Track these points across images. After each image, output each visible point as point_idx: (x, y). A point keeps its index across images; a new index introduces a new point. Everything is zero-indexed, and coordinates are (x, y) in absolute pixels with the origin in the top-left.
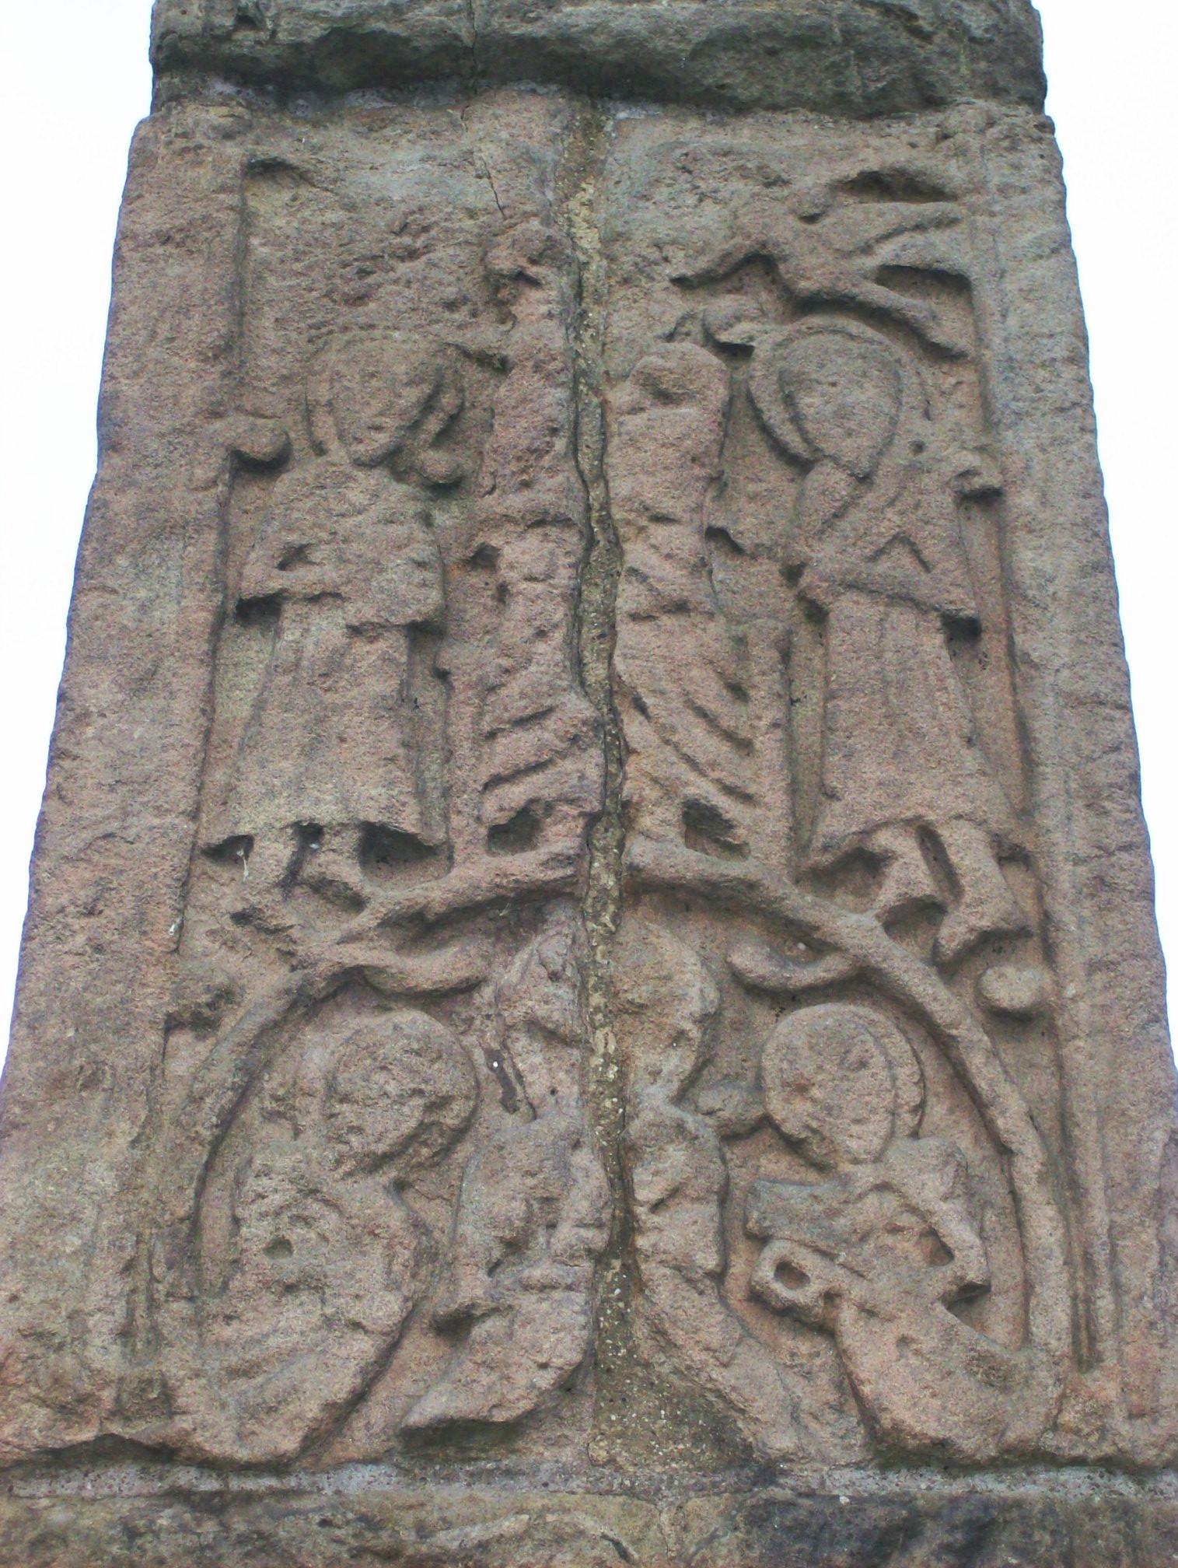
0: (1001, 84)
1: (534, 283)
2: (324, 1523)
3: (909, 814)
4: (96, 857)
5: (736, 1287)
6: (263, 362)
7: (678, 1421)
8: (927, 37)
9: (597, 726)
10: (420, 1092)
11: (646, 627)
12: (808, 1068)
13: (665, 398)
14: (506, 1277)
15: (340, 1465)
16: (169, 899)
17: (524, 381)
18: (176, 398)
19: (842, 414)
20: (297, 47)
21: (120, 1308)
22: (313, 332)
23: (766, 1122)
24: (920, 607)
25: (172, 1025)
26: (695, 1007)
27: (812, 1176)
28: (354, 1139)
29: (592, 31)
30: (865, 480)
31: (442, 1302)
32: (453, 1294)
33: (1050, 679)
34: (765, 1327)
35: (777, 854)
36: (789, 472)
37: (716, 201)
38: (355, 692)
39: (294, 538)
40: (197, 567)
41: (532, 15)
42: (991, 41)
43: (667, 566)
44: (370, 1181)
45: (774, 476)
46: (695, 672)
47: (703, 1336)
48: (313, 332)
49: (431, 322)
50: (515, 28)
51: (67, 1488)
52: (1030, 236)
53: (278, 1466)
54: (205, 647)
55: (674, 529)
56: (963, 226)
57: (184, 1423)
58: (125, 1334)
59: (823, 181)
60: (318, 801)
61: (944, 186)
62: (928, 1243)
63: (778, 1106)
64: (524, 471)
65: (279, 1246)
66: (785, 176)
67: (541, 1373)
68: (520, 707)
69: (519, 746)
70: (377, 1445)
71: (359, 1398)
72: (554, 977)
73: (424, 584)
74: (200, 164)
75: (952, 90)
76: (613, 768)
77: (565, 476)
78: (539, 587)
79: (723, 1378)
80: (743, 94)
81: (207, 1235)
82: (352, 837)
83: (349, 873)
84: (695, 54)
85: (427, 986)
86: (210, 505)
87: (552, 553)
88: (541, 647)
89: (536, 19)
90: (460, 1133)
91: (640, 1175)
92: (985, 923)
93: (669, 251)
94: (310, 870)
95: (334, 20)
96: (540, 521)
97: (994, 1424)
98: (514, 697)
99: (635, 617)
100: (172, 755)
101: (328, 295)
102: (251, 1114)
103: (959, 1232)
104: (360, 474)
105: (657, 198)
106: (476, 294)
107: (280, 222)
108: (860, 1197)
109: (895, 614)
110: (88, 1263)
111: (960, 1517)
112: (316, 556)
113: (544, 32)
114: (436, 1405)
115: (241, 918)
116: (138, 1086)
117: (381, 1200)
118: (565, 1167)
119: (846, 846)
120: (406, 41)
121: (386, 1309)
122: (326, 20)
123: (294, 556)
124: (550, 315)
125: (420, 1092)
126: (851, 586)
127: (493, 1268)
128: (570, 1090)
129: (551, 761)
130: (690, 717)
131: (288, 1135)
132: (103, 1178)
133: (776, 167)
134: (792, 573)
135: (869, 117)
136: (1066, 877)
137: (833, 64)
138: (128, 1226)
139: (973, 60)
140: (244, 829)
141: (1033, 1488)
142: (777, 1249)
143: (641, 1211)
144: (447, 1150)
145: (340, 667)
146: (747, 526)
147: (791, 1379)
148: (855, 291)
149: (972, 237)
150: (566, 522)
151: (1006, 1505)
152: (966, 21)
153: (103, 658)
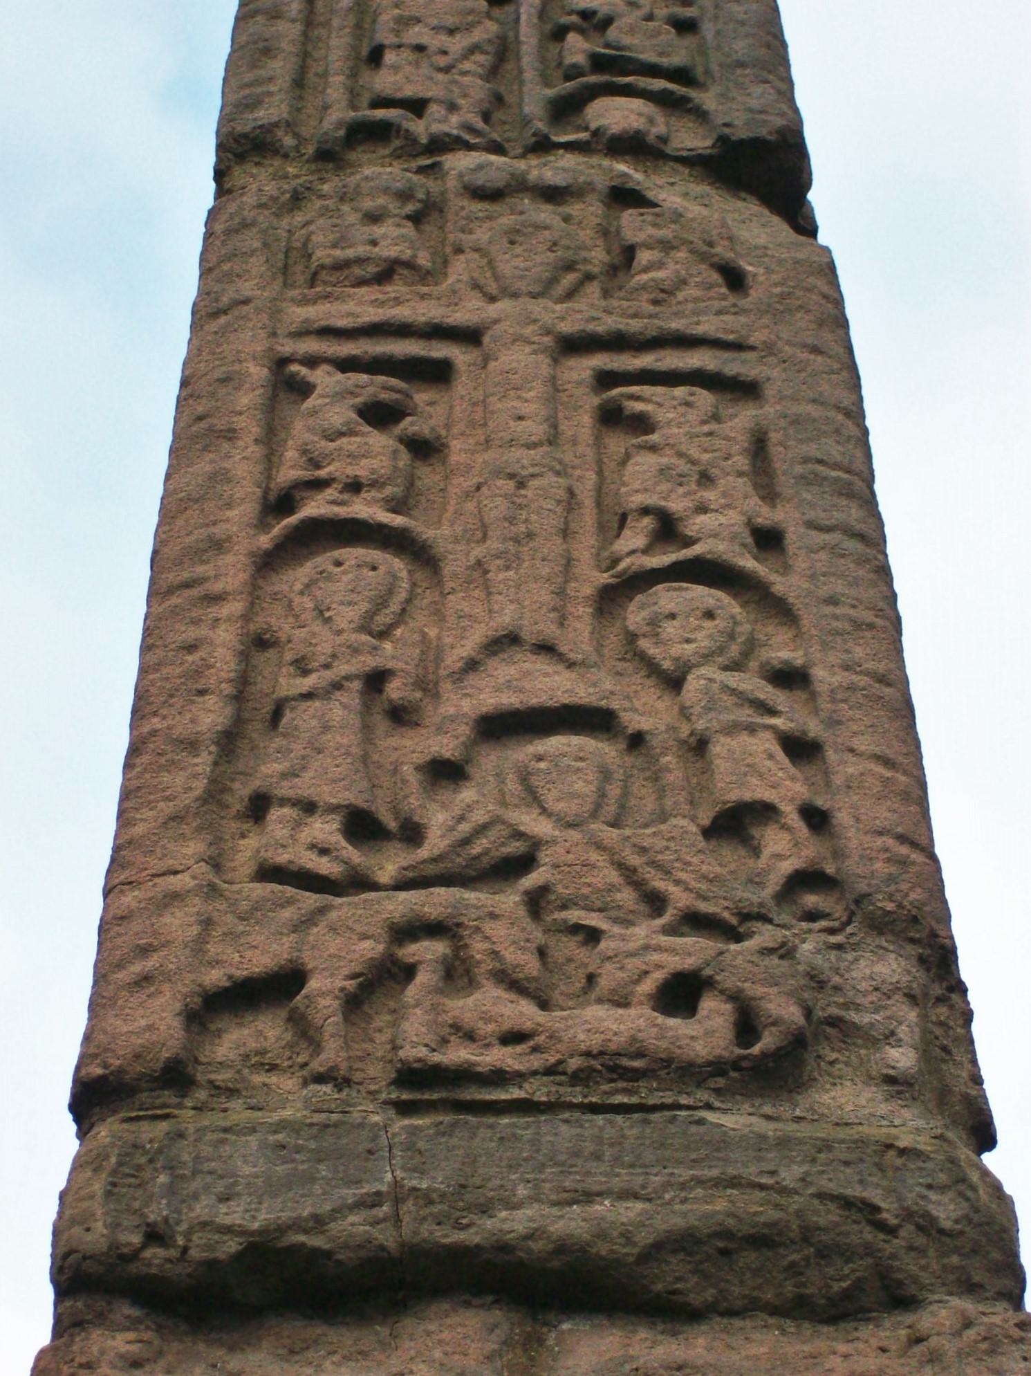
8: (892, 1231)
20: (212, 1264)
42: (962, 1233)
50: (446, 1236)
75: (922, 1287)
80: (695, 1299)
95: (252, 1233)
113: (477, 1239)
120: (328, 1254)
137: (792, 1265)
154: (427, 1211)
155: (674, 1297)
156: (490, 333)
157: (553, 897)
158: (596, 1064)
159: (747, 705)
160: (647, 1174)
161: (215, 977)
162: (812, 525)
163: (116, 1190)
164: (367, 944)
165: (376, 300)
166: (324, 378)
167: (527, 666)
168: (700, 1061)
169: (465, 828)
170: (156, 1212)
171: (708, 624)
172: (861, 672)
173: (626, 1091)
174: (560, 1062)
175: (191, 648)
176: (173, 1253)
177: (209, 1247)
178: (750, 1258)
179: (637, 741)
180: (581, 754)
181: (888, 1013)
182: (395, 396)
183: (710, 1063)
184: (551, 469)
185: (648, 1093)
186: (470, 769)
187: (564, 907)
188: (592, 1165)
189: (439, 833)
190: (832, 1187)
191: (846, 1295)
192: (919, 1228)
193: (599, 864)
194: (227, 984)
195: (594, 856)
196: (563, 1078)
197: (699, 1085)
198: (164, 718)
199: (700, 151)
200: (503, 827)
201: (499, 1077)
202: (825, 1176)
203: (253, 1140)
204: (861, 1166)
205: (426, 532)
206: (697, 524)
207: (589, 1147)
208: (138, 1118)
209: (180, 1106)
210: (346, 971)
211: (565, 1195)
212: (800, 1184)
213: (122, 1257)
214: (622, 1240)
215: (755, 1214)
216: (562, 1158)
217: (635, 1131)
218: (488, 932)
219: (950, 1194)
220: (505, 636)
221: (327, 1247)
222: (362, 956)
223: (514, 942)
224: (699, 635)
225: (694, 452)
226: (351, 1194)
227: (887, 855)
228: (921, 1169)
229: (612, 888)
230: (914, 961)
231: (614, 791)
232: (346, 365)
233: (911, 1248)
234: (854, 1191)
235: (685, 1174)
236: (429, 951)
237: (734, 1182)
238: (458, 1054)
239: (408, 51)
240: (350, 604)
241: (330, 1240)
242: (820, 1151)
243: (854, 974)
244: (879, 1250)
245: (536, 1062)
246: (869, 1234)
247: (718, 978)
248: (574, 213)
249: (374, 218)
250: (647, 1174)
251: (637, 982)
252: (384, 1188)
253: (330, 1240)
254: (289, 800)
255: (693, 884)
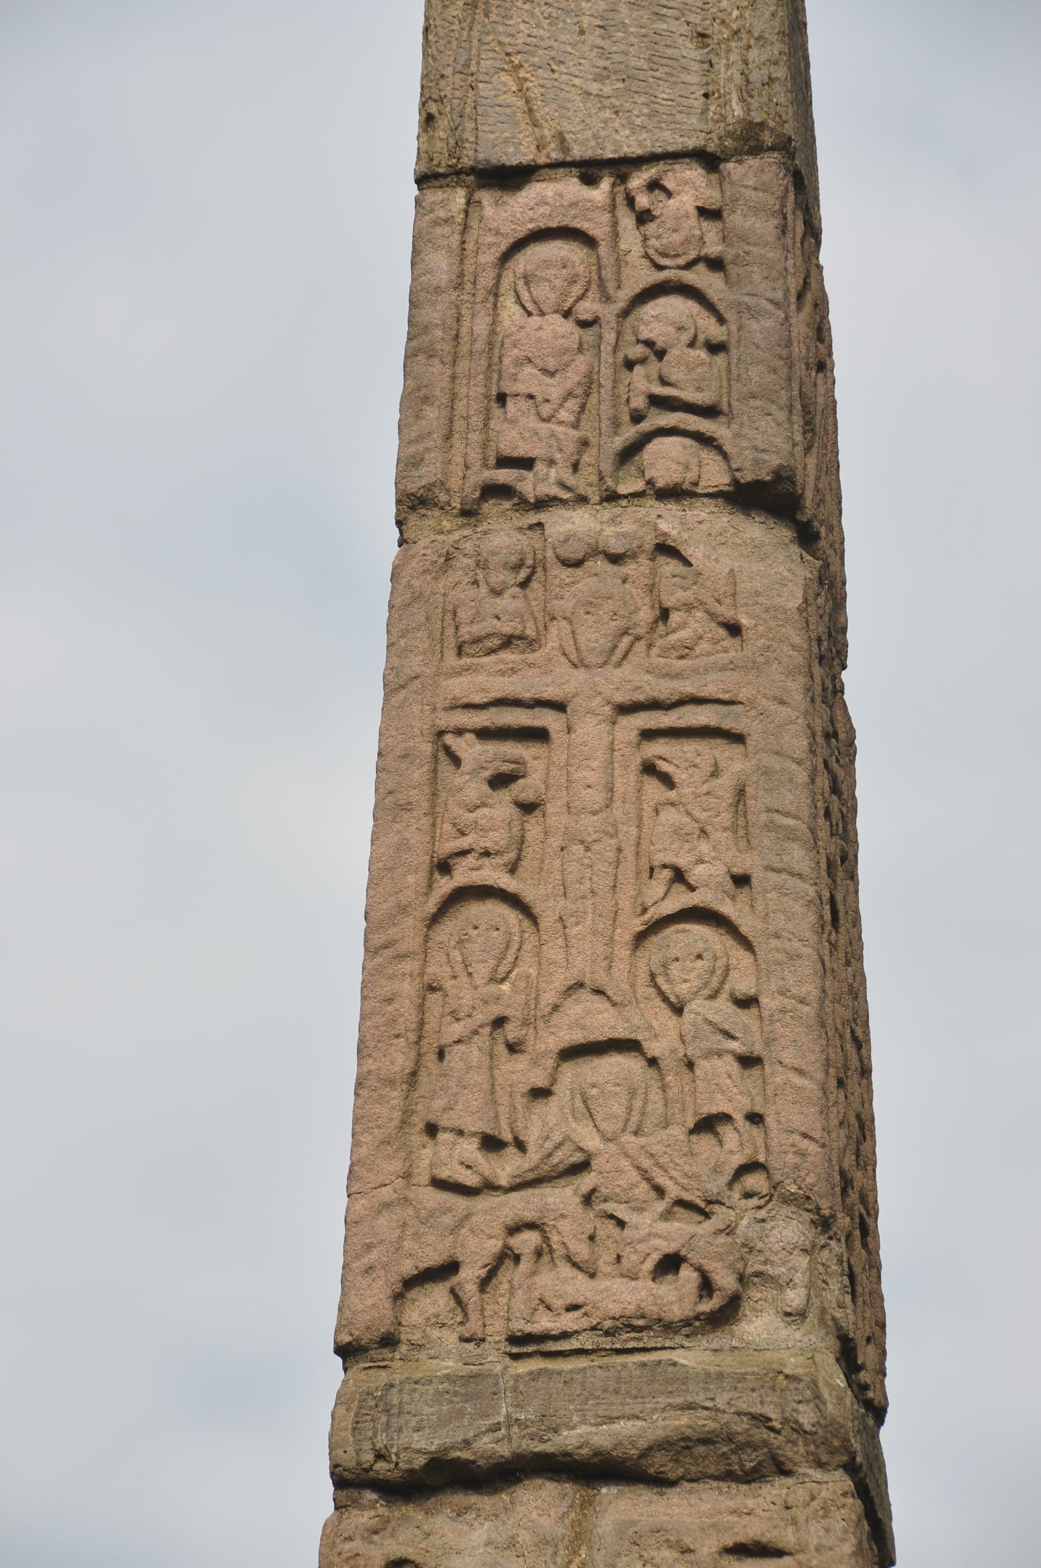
8: (778, 1432)
20: (412, 1471)
29: (579, 1447)
41: (545, 1438)
42: (816, 1433)
44: (534, 1245)
50: (536, 1447)
59: (714, 1550)
61: (784, 1547)
66: (692, 1547)
67: (670, 1247)
75: (795, 1464)
80: (672, 1476)
89: (549, 1440)
95: (431, 1453)
120: (474, 1462)
122: (425, 1453)
133: (687, 1541)
137: (724, 1454)
139: (806, 1445)
154: (525, 1431)
155: (661, 1475)
156: (571, 704)
157: (598, 1194)
159: (718, 1033)
160: (644, 1403)
161: (409, 1268)
162: (770, 868)
163: (360, 1425)
164: (493, 1241)
165: (500, 670)
166: (469, 749)
167: (588, 1004)
168: (676, 1319)
169: (549, 1145)
170: (381, 1441)
171: (699, 963)
172: (791, 997)
173: (635, 1339)
174: (598, 1323)
175: (389, 1001)
176: (392, 1466)
177: (410, 1462)
178: (701, 1449)
179: (653, 1062)
180: (618, 1081)
181: (790, 1265)
182: (513, 766)
183: (682, 1321)
184: (607, 833)
185: (648, 1340)
186: (553, 1088)
187: (605, 1201)
188: (613, 1398)
189: (534, 1150)
190: (743, 1406)
191: (754, 1469)
193: (626, 1169)
194: (416, 1272)
195: (624, 1163)
196: (601, 1332)
198: (375, 1060)
199: (721, 488)
200: (571, 1143)
201: (565, 1335)
202: (741, 1400)
203: (431, 1389)
204: (762, 1391)
205: (529, 894)
206: (697, 873)
207: (612, 1385)
208: (370, 1367)
209: (392, 1360)
210: (480, 1263)
211: (599, 1420)
212: (727, 1406)
213: (364, 1470)
214: (630, 1447)
215: (704, 1426)
216: (597, 1393)
217: (638, 1373)
218: (561, 1229)
219: (812, 1405)
220: (575, 984)
221: (472, 1458)
222: (489, 1252)
223: (575, 1236)
224: (692, 976)
225: (697, 813)
226: (485, 1423)
227: (794, 1149)
229: (634, 1186)
230: (807, 1225)
231: (638, 1104)
232: (484, 734)
233: (789, 1441)
234: (757, 1409)
235: (663, 1401)
236: (528, 1241)
237: (690, 1407)
239: (523, 399)
240: (483, 961)
241: (475, 1453)
242: (739, 1382)
243: (772, 1239)
244: (771, 1444)
245: (585, 1323)
246: (766, 1434)
247: (689, 1256)
248: (631, 573)
249: (497, 593)
250: (644, 1403)
251: (643, 1262)
252: (502, 1419)
253: (475, 1453)
254: (448, 1128)
255: (680, 1180)
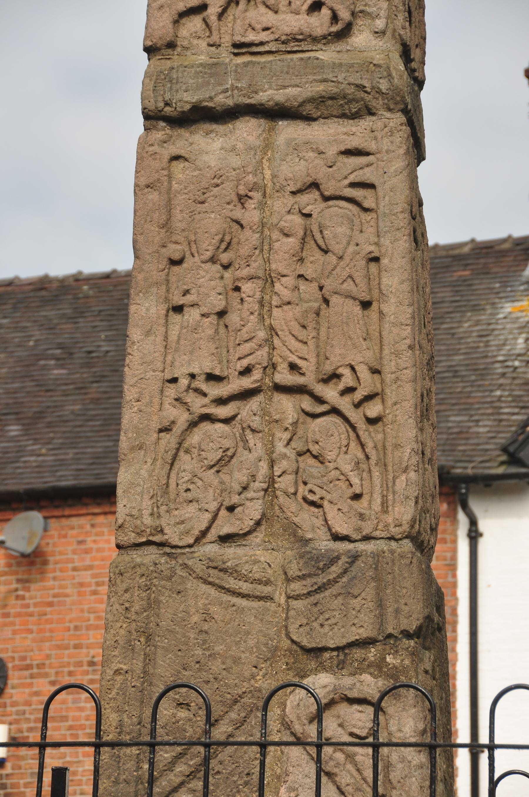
0: (392, 107)
1: (250, 198)
2: (200, 560)
3: (347, 363)
4: (139, 385)
5: (300, 496)
6: (177, 225)
7: (285, 531)
8: (369, 93)
9: (267, 340)
10: (221, 448)
11: (280, 309)
12: (318, 438)
13: (287, 235)
14: (243, 496)
15: (204, 544)
16: (158, 396)
17: (248, 232)
18: (153, 242)
19: (335, 236)
20: (183, 112)
21: (150, 508)
22: (191, 214)
23: (308, 451)
24: (354, 299)
25: (161, 431)
26: (290, 421)
27: (320, 465)
28: (205, 461)
30: (341, 258)
31: (227, 503)
32: (230, 501)
33: (388, 319)
34: (306, 506)
35: (313, 377)
36: (322, 253)
37: (304, 160)
38: (203, 334)
39: (185, 287)
40: (160, 297)
43: (285, 290)
45: (318, 254)
46: (292, 323)
47: (291, 509)
48: (191, 214)
49: (223, 210)
51: (140, 552)
52: (394, 168)
53: (190, 546)
54: (164, 321)
55: (287, 278)
56: (375, 165)
57: (166, 537)
58: (152, 514)
60: (194, 367)
62: (347, 482)
63: (312, 448)
64: (247, 262)
65: (188, 490)
68: (246, 336)
69: (247, 347)
70: (213, 539)
71: (208, 529)
72: (255, 414)
73: (220, 300)
74: (155, 159)
76: (271, 352)
77: (260, 261)
78: (251, 299)
79: (296, 520)
80: (315, 116)
81: (171, 487)
82: (203, 377)
83: (204, 387)
84: (299, 106)
85: (223, 418)
86: (164, 277)
87: (255, 288)
88: (252, 317)
90: (232, 457)
91: (275, 468)
92: (366, 394)
93: (289, 182)
94: (193, 386)
96: (251, 278)
97: (359, 530)
98: (244, 334)
99: (277, 307)
100: (156, 354)
101: (194, 201)
102: (181, 453)
103: (355, 480)
104: (203, 265)
105: (287, 160)
106: (235, 199)
107: (181, 176)
108: (330, 472)
109: (347, 300)
110: (142, 497)
111: (350, 555)
112: (192, 292)
113: (254, 102)
114: (225, 530)
115: (176, 400)
116: (152, 449)
117: (212, 477)
118: (257, 467)
119: (330, 373)
120: (215, 108)
121: (213, 506)
123: (186, 292)
124: (255, 208)
125: (221, 448)
126: (335, 293)
127: (240, 494)
128: (259, 445)
129: (254, 352)
130: (291, 336)
131: (190, 458)
132: (144, 473)
133: (322, 148)
134: (321, 288)
135: (353, 119)
136: (389, 378)
137: (341, 104)
138: (151, 487)
139: (383, 100)
140: (176, 376)
141: (369, 547)
142: (309, 486)
143: (275, 478)
144: (229, 461)
145: (199, 326)
146: (309, 272)
147: (313, 518)
148: (341, 193)
149: (377, 170)
150: (259, 278)
151: (363, 551)
152: (381, 87)
153: (137, 325)
158: (289, 38)
168: (319, 35)
170: (167, 97)
173: (297, 46)
176: (173, 109)
177: (182, 107)
178: (330, 102)
185: (304, 46)
191: (357, 112)
192: (377, 92)
197: (319, 43)
201: (262, 44)
203: (193, 70)
207: (285, 69)
209: (173, 55)
210: (218, 5)
216: (278, 74)
219: (387, 80)
226: (220, 88)
228: (379, 71)
234: (359, 82)
237: (325, 81)
238: (251, 37)
241: (215, 104)
245: (272, 37)
252: (229, 86)
253: (215, 104)
